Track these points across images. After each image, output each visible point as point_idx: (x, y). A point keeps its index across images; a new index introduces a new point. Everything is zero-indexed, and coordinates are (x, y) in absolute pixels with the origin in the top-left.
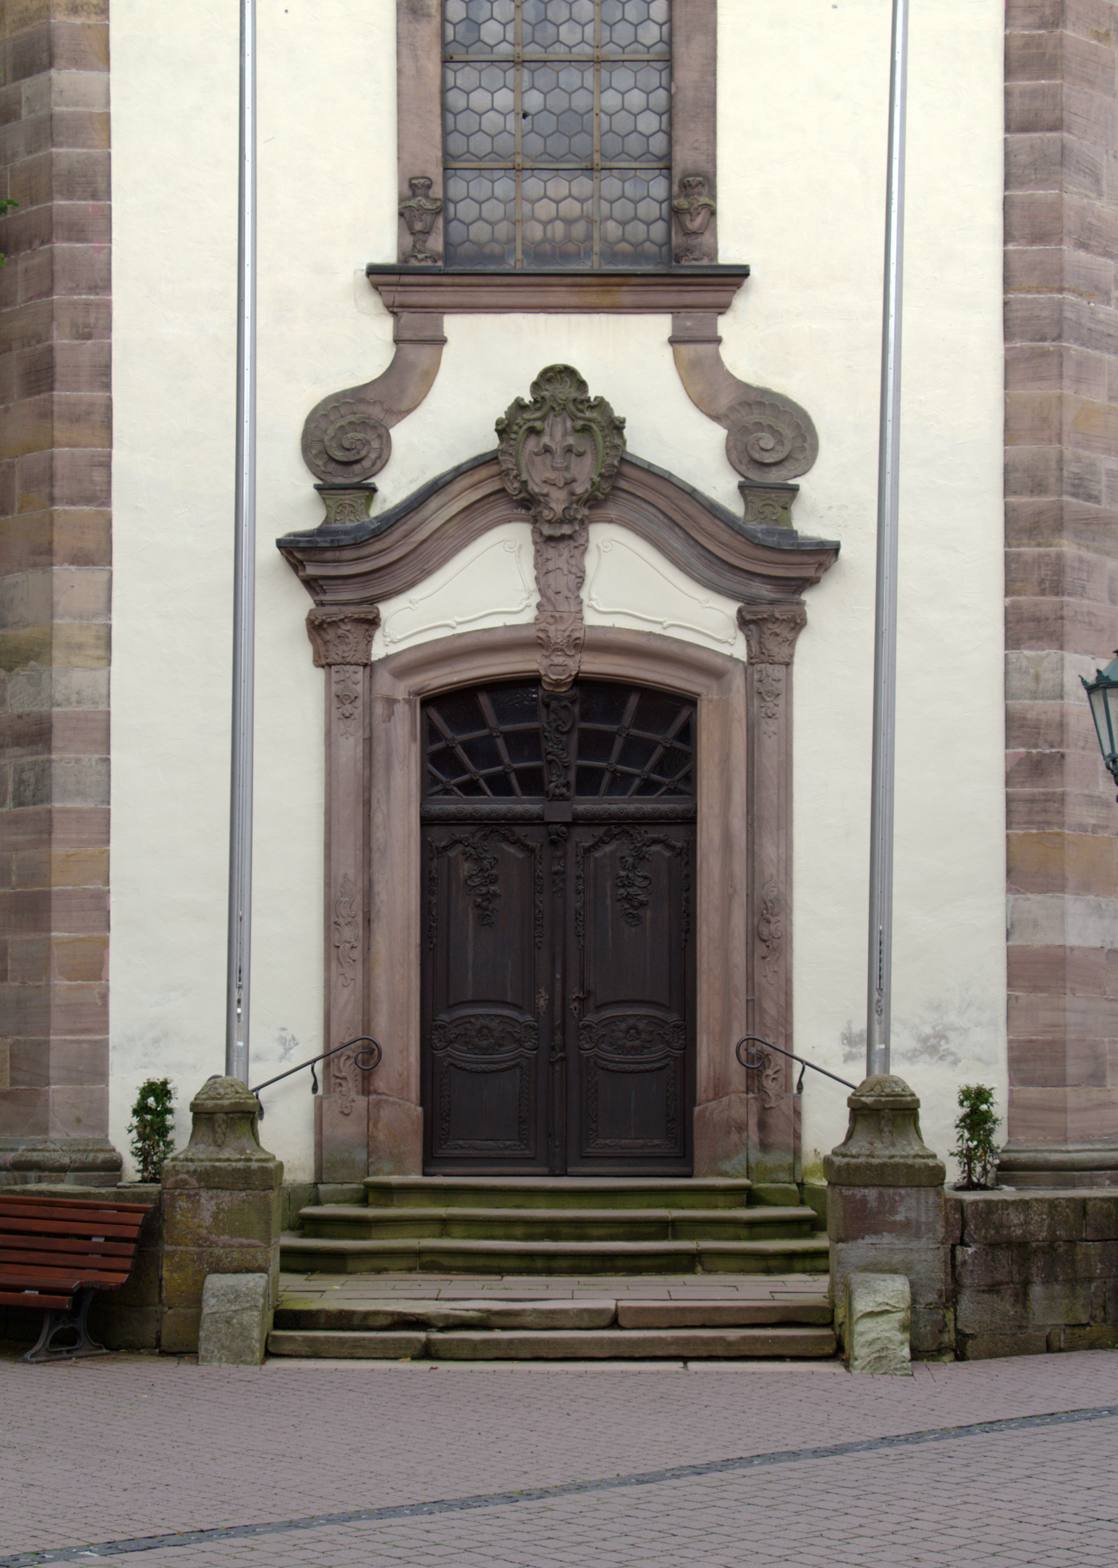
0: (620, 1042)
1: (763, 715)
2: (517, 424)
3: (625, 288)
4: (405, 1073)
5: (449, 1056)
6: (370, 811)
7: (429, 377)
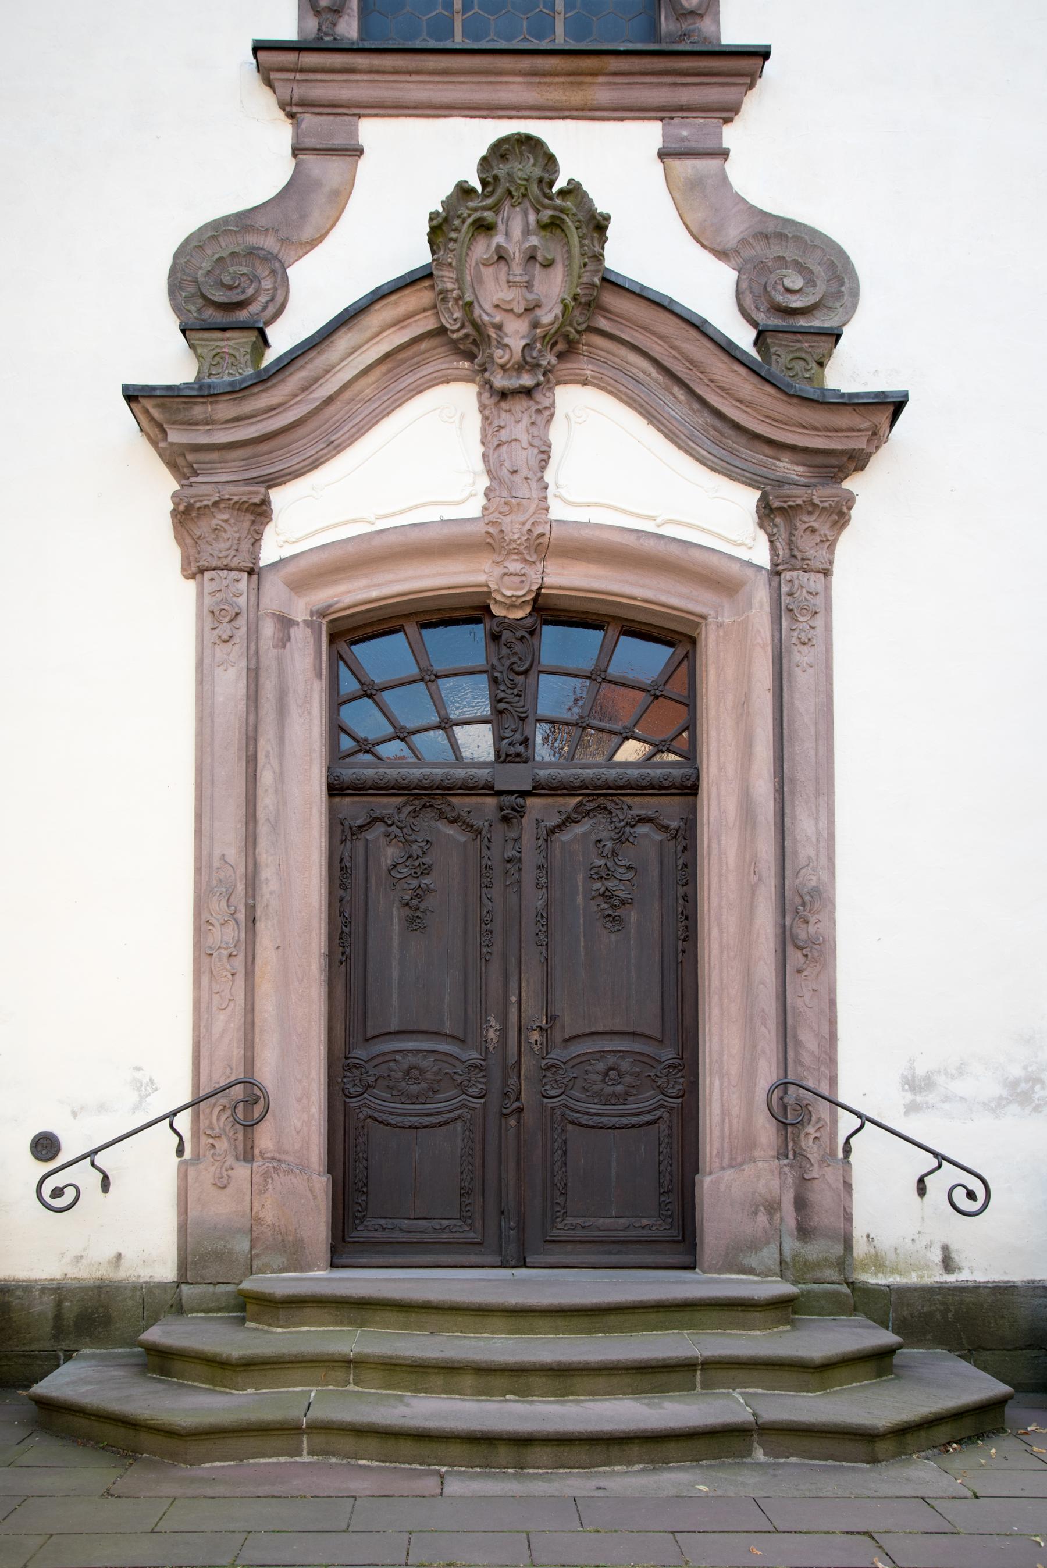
0: (596, 1088)
1: (794, 640)
2: (459, 217)
3: (601, 79)
4: (305, 1129)
5: (366, 1105)
6: (255, 771)
7: (340, 198)
